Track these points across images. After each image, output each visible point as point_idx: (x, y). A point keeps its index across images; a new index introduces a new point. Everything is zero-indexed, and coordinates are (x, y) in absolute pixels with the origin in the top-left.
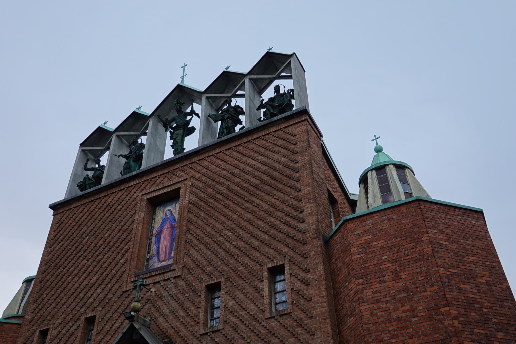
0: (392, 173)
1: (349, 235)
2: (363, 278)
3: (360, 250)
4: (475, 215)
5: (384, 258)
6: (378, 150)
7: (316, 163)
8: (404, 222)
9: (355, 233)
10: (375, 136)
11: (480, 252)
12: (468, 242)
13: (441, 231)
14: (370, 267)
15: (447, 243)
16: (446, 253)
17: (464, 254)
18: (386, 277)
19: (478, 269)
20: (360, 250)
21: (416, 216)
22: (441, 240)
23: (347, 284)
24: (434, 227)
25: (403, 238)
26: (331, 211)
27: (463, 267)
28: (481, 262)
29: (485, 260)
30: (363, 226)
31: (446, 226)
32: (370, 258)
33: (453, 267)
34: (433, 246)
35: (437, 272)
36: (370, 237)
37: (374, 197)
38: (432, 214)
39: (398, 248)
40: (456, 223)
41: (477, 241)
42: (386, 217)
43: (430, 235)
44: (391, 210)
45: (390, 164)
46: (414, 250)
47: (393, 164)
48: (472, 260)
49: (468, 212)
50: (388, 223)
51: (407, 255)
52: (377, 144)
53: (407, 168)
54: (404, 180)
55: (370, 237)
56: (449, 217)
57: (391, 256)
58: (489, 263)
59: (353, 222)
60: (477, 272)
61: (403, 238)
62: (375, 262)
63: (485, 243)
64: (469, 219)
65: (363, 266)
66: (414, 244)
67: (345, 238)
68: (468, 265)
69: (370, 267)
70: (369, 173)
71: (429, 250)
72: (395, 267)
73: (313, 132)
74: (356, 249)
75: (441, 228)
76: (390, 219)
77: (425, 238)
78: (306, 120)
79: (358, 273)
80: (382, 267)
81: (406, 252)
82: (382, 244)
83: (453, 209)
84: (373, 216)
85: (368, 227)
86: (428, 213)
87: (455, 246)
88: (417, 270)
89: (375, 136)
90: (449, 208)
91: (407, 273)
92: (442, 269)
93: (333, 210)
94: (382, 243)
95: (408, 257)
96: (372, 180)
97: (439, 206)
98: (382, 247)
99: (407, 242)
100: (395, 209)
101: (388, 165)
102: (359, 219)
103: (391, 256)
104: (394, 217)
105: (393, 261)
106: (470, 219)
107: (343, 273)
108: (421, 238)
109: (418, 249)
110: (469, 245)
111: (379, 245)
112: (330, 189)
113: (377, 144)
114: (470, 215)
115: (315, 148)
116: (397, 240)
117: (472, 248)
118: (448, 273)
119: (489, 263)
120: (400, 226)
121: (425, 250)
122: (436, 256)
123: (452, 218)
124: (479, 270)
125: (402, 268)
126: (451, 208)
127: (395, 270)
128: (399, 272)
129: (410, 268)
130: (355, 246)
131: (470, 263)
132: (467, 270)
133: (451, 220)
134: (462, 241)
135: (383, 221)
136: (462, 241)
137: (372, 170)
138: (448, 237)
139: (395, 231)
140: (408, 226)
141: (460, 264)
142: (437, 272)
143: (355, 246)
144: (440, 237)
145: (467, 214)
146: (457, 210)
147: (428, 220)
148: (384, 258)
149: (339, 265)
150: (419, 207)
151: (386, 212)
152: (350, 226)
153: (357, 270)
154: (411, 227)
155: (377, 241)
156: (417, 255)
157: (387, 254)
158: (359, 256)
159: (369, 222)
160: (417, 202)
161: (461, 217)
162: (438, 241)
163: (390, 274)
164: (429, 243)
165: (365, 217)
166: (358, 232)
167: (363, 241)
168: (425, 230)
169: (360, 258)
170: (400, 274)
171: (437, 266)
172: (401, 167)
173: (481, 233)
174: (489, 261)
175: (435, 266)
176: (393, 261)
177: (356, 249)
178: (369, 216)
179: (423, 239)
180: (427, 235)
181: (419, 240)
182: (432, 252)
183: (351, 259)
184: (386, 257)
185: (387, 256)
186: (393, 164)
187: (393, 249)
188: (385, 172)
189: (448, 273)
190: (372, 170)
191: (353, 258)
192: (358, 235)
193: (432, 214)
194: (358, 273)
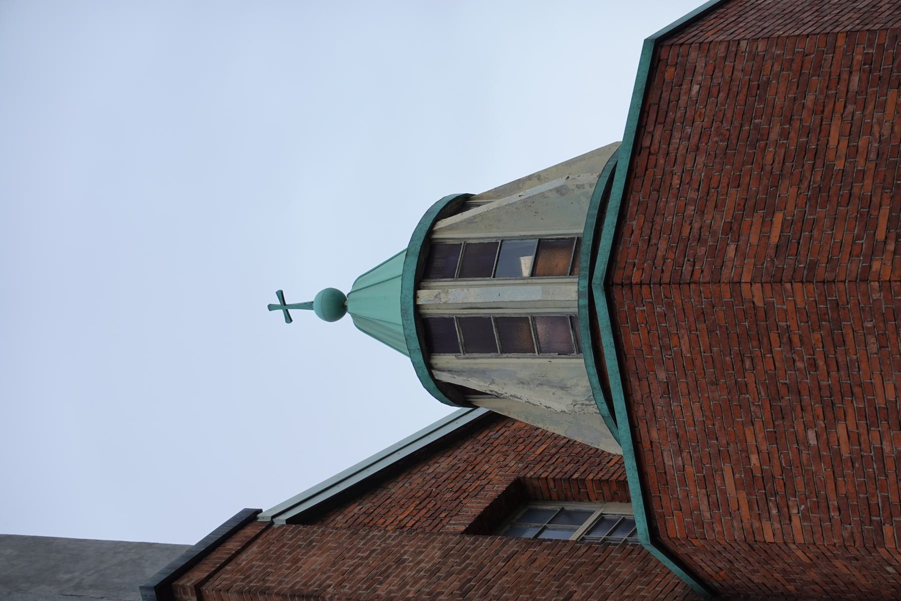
0: (452, 297)
1: (710, 536)
2: (881, 524)
3: (774, 512)
4: (667, 76)
5: (813, 441)
6: (335, 305)
7: (386, 574)
8: (685, 347)
9: (708, 515)
10: (271, 307)
11: (810, 98)
12: (774, 136)
13: (729, 228)
14: (842, 491)
15: (778, 217)
16: (815, 232)
17: (819, 162)
18: (887, 448)
19: (876, 129)
20: (774, 512)
21: (670, 305)
22: (764, 237)
23: (890, 569)
24: (716, 252)
25: (748, 364)
26: (556, 507)
27: (868, 182)
28: (850, 108)
29: (842, 87)
30: (683, 482)
31: (711, 205)
32: (806, 485)
33: (868, 223)
34: (787, 274)
35: (886, 286)
36: (727, 468)
37: (543, 382)
38: (662, 246)
39: (783, 390)
40: (701, 160)
41: (769, 97)
42: (660, 404)
43: (746, 278)
44: (633, 380)
45: (415, 297)
46: (796, 339)
47: (418, 287)
48: (844, 143)
49: (653, 99)
50: (683, 401)
51: (814, 365)
52: (308, 306)
53: (431, 231)
54: (483, 261)
55: (727, 468)
56: (676, 181)
57: (808, 417)
58: (855, 79)
59: (663, 516)
60: (886, 132)
61: (748, 364)
62: (824, 470)
63: (777, 67)
64: (682, 102)
65: (835, 514)
66: (774, 335)
67: (718, 548)
68: (861, 160)
69: (842, 491)
70: (445, 377)
71: (802, 295)
72: (850, 412)
73: (243, 556)
74: (767, 525)
75: (719, 225)
76: (669, 389)
77: (757, 295)
78: (198, 588)
79: (858, 536)
80: (846, 455)
81: (799, 365)
82: (760, 436)
83: (644, 154)
84: (646, 445)
85: (690, 470)
86: (659, 261)
87: (788, 191)
88: (873, 347)
89: (271, 307)
90: (639, 171)
91: (877, 381)
92: (876, 266)
93: (550, 500)
94: (756, 437)
95: (821, 363)
96: (472, 373)
97: (632, 208)
98: (773, 438)
99: (763, 357)
100: (630, 365)
101: (417, 308)
102: (654, 493)
103: (808, 417)
104: (662, 376)
105: (830, 415)
106: (684, 98)
107: (846, 571)
108: (755, 307)
109: (794, 327)
110: (785, 134)
111: (764, 447)
112: (474, 508)
113: (308, 306)
114: (665, 95)
115: (315, 563)
116: (752, 386)
117: (796, 124)
118: (891, 247)
119: (855, 79)
120: (698, 362)
121: (801, 305)
122: (829, 276)
123: (677, 169)
124: (880, 125)
125: (857, 390)
126: (641, 160)
127: (861, 414)
128: (872, 403)
129: (863, 366)
130: (756, 525)
131: (853, 152)
132: (882, 169)
133: (686, 179)
134: (769, 158)
135: (671, 414)
136: (769, 158)
137: (430, 367)
138: (755, 209)
139: (715, 383)
140: (704, 340)
141: (856, 190)
142: (886, 286)
143: (756, 525)
144: (754, 240)
145: (663, 106)
146: (646, 142)
147: (687, 268)
148: (813, 441)
149: (812, 575)
150: (636, 289)
151: (637, 396)
152: (674, 527)
153: (846, 534)
154: (710, 331)
155: (746, 450)
156: (817, 335)
157: (799, 427)
158: (796, 521)
159: (668, 462)
160: (616, 292)
161: (677, 135)
162: (772, 252)
163: (875, 435)
164: (777, 287)
165: (650, 470)
166: (704, 507)
167: (743, 495)
168: (726, 289)
169: (805, 518)
170: (880, 403)
171: (865, 280)
172: (431, 256)
173: (738, 74)
174: (845, 76)
175: (863, 286)
176: (830, 415)
177: (767, 525)
178: (648, 457)
179: (759, 304)
180: (745, 288)
181: (761, 314)
182: (811, 287)
183: (803, 547)
184: (811, 435)
185: (806, 428)
186: (418, 287)
187: (783, 403)
188: (454, 248)
189: (891, 247)
190: (430, 367)
191: (799, 539)
192: (714, 505)
193: (662, 246)
194: (858, 536)
